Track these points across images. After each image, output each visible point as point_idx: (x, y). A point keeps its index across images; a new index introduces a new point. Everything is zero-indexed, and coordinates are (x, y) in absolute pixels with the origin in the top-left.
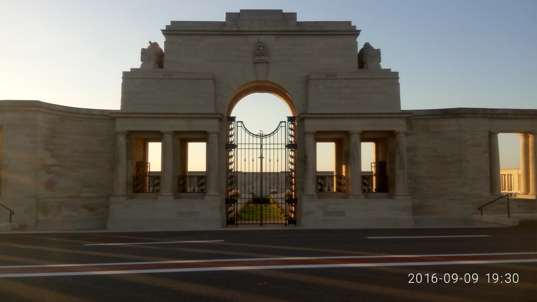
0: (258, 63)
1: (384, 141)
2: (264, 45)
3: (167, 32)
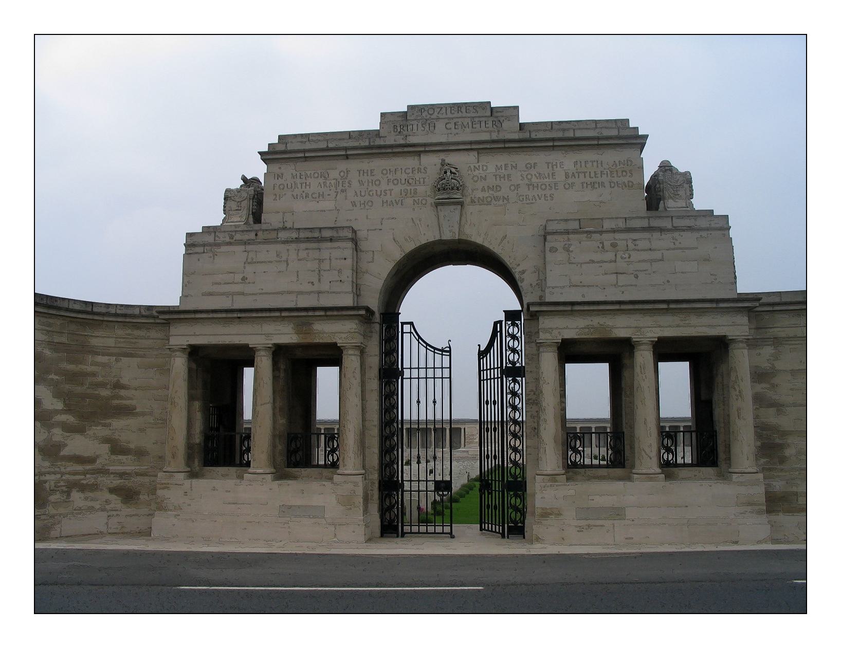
0: (442, 204)
1: (706, 360)
2: (453, 170)
3: (266, 157)
